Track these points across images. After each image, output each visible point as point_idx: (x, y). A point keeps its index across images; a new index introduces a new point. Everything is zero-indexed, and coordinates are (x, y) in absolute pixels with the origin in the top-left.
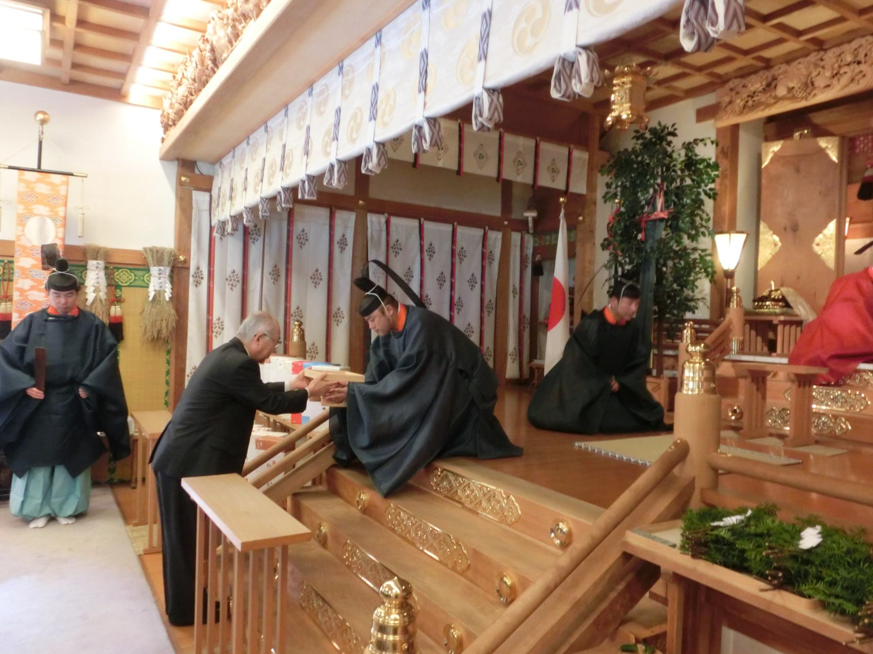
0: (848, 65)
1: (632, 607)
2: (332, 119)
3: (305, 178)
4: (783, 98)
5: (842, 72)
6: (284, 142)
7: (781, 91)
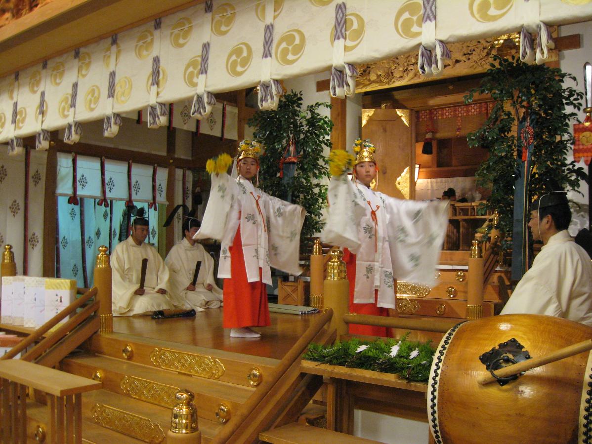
0: (413, 65)
1: (304, 407)
2: (70, 91)
3: (41, 131)
4: (374, 82)
5: (409, 69)
6: (15, 100)
7: (373, 77)
